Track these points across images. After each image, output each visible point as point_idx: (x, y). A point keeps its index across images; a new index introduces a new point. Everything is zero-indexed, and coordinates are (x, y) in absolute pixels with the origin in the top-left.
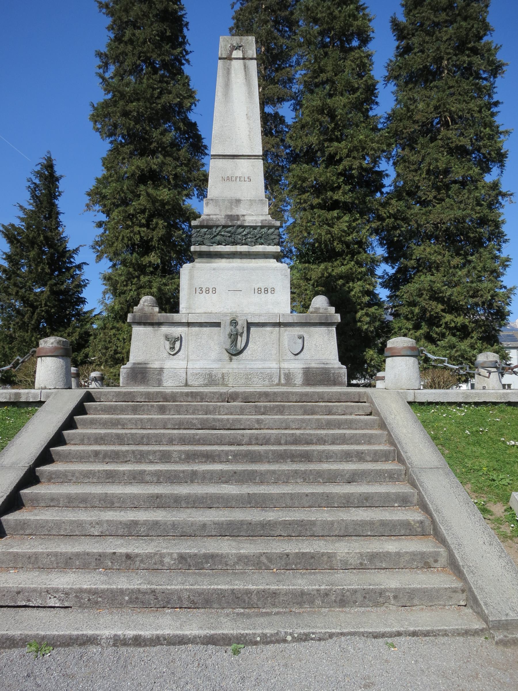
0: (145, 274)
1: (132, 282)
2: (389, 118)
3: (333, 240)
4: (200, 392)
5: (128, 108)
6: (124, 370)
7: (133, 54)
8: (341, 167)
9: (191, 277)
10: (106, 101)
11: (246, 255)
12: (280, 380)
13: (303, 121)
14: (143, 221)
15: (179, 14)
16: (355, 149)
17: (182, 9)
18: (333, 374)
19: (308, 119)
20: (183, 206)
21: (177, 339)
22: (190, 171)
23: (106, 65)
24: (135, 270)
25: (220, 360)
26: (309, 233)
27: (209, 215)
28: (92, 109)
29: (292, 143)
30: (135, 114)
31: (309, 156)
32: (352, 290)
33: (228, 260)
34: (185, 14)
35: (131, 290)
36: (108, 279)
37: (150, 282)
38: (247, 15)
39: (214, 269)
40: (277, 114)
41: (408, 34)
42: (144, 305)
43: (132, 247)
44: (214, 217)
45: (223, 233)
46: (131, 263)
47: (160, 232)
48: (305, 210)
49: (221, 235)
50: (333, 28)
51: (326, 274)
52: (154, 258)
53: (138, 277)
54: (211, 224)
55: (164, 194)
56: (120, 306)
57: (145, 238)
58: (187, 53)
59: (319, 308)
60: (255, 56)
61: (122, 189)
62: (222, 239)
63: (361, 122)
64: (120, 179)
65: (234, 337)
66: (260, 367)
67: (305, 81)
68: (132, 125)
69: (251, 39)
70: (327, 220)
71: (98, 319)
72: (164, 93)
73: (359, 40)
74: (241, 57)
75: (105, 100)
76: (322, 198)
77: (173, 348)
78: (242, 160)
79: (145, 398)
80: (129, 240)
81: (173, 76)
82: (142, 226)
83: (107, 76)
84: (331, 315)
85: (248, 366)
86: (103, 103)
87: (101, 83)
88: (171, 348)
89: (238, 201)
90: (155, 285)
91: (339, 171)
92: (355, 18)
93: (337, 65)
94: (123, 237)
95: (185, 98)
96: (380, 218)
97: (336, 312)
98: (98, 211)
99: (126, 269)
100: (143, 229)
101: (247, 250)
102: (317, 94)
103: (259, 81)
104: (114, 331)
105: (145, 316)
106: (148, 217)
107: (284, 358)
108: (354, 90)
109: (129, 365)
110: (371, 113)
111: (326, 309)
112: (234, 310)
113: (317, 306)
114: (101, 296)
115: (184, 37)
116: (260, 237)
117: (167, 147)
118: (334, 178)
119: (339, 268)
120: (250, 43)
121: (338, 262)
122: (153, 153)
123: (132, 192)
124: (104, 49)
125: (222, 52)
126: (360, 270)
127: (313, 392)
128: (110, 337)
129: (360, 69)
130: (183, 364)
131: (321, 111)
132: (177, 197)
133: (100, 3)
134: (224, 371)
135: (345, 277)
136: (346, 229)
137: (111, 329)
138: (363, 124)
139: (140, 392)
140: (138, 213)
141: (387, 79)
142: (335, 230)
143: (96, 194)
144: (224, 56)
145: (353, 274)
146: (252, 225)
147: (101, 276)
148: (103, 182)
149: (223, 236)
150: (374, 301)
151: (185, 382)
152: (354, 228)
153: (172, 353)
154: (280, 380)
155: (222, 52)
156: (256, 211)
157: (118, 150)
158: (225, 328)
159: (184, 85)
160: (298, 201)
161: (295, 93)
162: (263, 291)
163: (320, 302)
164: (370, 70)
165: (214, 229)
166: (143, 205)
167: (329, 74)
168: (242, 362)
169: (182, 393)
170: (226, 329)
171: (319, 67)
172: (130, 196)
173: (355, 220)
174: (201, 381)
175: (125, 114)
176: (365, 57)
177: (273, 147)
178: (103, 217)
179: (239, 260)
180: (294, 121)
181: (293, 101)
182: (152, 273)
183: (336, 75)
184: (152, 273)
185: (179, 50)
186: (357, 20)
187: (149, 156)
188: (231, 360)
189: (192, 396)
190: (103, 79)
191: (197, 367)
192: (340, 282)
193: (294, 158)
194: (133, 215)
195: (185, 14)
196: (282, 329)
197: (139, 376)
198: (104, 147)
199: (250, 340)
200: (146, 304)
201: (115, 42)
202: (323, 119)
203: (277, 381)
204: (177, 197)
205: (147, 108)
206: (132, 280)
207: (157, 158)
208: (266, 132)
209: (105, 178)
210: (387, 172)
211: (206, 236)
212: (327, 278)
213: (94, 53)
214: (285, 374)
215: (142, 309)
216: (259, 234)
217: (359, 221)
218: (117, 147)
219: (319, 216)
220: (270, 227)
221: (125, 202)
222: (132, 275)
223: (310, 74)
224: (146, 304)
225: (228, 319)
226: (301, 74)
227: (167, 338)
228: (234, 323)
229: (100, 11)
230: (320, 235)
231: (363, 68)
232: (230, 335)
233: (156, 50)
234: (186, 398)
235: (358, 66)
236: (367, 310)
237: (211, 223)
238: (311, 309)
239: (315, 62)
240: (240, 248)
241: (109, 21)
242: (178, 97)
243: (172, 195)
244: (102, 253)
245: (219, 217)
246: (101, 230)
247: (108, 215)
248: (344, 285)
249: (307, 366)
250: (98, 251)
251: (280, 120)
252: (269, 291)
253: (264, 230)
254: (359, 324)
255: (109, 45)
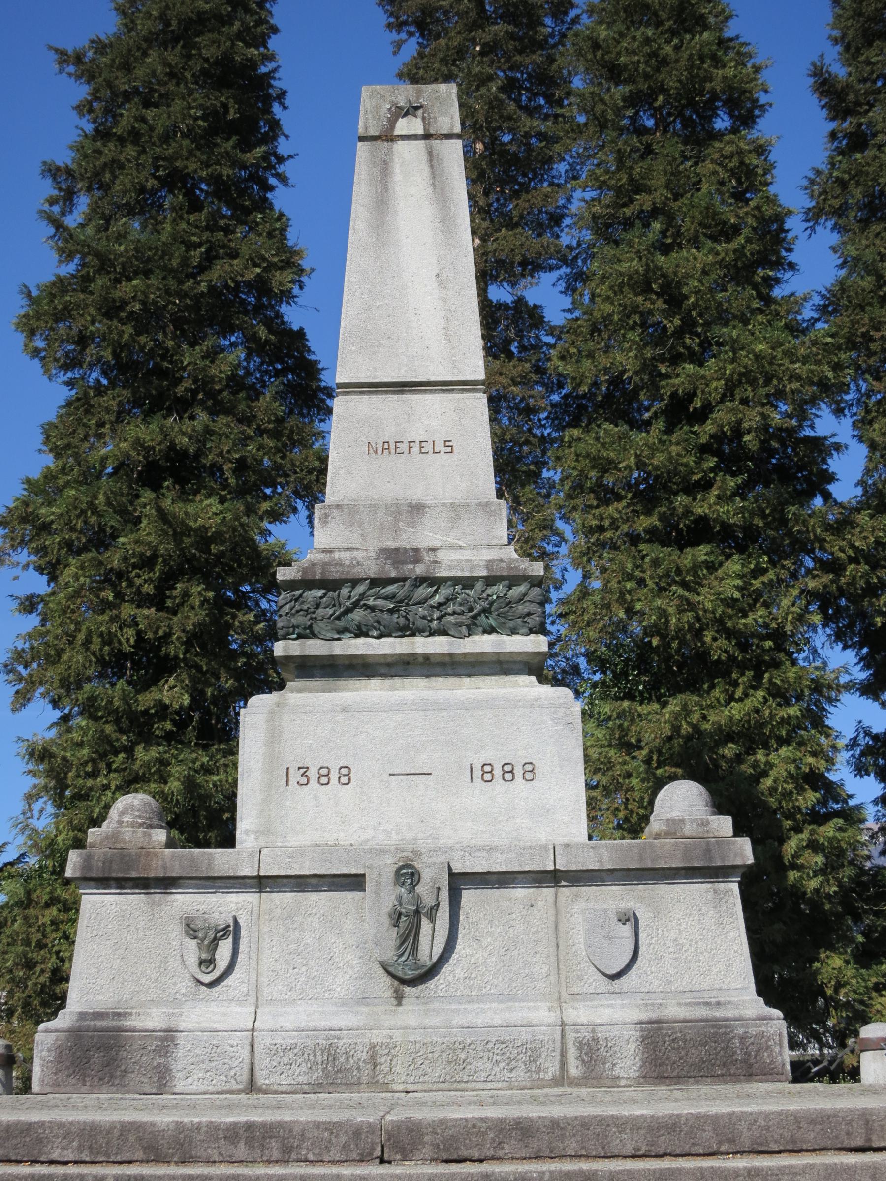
0: (147, 738)
1: (109, 765)
2: (825, 306)
3: (701, 630)
4: (280, 1125)
5: (117, 294)
6: (47, 1036)
7: (138, 165)
8: (709, 427)
9: (274, 737)
10: (60, 280)
11: (443, 664)
12: (563, 1064)
13: (597, 314)
14: (149, 589)
15: (263, 70)
16: (747, 378)
17: (271, 58)
18: (743, 1039)
19: (608, 308)
20: (262, 546)
21: (224, 932)
22: (282, 451)
23: (69, 197)
24: (121, 731)
25: (364, 1000)
26: (630, 612)
27: (330, 551)
28: (25, 302)
29: (566, 368)
30: (137, 307)
31: (617, 402)
32: (765, 774)
33: (388, 682)
34: (275, 70)
35: (106, 787)
36: (40, 754)
37: (163, 763)
38: (436, 65)
39: (344, 710)
40: (520, 301)
41: (858, 104)
42: (120, 822)
43: (113, 664)
44: (348, 555)
45: (371, 602)
46: (111, 711)
47: (193, 617)
48: (615, 547)
49: (367, 607)
50: (662, 89)
51: (685, 729)
52: (173, 693)
53: (129, 751)
54: (337, 576)
55: (207, 511)
56: (71, 834)
57: (150, 635)
58: (281, 160)
59: (682, 821)
60: (458, 129)
61: (92, 506)
62: (370, 617)
63: (754, 311)
64: (90, 476)
65: (408, 923)
66: (497, 1021)
67: (595, 217)
68: (126, 336)
69: (449, 91)
70: (679, 571)
71: (11, 876)
72: (217, 257)
73: (731, 116)
74: (421, 132)
75: (59, 277)
76: (660, 516)
77: (208, 963)
78: (428, 396)
79: (80, 1148)
80: (104, 643)
81: (242, 214)
82: (142, 601)
83: (72, 221)
84: (721, 842)
85: (457, 1020)
86: (54, 284)
87: (52, 237)
88: (201, 963)
89: (417, 509)
90: (176, 770)
91: (704, 439)
92: (717, 62)
93: (676, 174)
94: (90, 633)
95: (271, 267)
96: (834, 567)
97: (737, 832)
98: (26, 567)
99: (93, 726)
100: (146, 612)
101: (445, 650)
102: (630, 244)
103: (472, 221)
104: (54, 911)
105: (124, 857)
106: (160, 579)
107: (576, 990)
108: (728, 232)
109: (64, 1020)
110: (777, 292)
111: (704, 823)
112: (409, 835)
113: (675, 814)
114: (21, 805)
115: (275, 125)
116: (486, 611)
117: (220, 391)
118: (691, 460)
119: (726, 710)
120: (445, 102)
121: (716, 693)
122: (183, 407)
123: (122, 512)
124: (65, 158)
125: (368, 121)
126: (783, 713)
127: (698, 1117)
128: (42, 929)
129: (740, 182)
130: (240, 1016)
131: (643, 285)
132: (245, 519)
133: (62, 53)
134: (378, 1036)
135: (740, 734)
136: (737, 595)
137: (47, 906)
138: (760, 318)
139: (61, 1125)
140: (135, 567)
141: (814, 216)
142: (705, 599)
143: (24, 520)
144: (372, 132)
145: (763, 725)
146: (459, 574)
147: (22, 748)
148: (44, 487)
149: (373, 609)
150: (833, 806)
151: (245, 1077)
152: (758, 594)
153: (207, 979)
154: (563, 1064)
155: (368, 121)
156: (473, 538)
157: (87, 403)
158: (377, 893)
159: (270, 235)
160: (594, 522)
161: (570, 248)
162: (498, 772)
163: (682, 802)
164: (767, 184)
165: (345, 591)
166: (149, 543)
167: (660, 195)
168: (435, 1005)
169: (213, 1128)
170: (384, 895)
171: (631, 180)
172: (112, 523)
173: (759, 572)
174: (301, 1074)
175: (112, 310)
176: (750, 152)
177: (515, 384)
178: (39, 585)
179: (421, 682)
180: (569, 316)
181: (565, 270)
182: (169, 737)
183: (677, 197)
184: (169, 737)
185: (259, 151)
186: (724, 66)
187: (169, 414)
188: (399, 998)
189: (250, 1142)
190: (58, 226)
191: (288, 1025)
192: (730, 750)
193: (575, 412)
194: (120, 575)
195: (275, 70)
196: (566, 892)
197: (97, 1058)
198: (49, 396)
199: (461, 931)
200: (127, 819)
201: (94, 139)
202: (648, 305)
203: (552, 1069)
204: (245, 519)
205: (168, 292)
206: (111, 757)
207: (192, 418)
208: (495, 348)
209: (49, 476)
210: (835, 440)
211: (320, 612)
212: (689, 738)
213: (38, 168)
214: (580, 1045)
215: (115, 836)
216: (480, 602)
217: (771, 575)
218: (86, 394)
219: (656, 563)
220: (513, 580)
221: (102, 540)
222: (110, 743)
223: (609, 197)
224: (127, 819)
225: (389, 864)
226: (583, 200)
227: (191, 929)
228: (407, 874)
229: (61, 71)
230: (663, 613)
231: (747, 178)
232: (396, 917)
233: (198, 153)
234: (228, 1149)
235: (733, 173)
236: (812, 833)
237: (335, 574)
238: (655, 824)
239: (618, 169)
240: (422, 645)
241: (82, 91)
242: (255, 265)
243: (229, 516)
244: (32, 683)
245: (359, 555)
246: (33, 621)
247: (53, 578)
248: (739, 759)
249: (654, 1016)
250: (20, 679)
251: (531, 316)
252: (519, 771)
253: (499, 589)
254: (793, 875)
255: (79, 148)
